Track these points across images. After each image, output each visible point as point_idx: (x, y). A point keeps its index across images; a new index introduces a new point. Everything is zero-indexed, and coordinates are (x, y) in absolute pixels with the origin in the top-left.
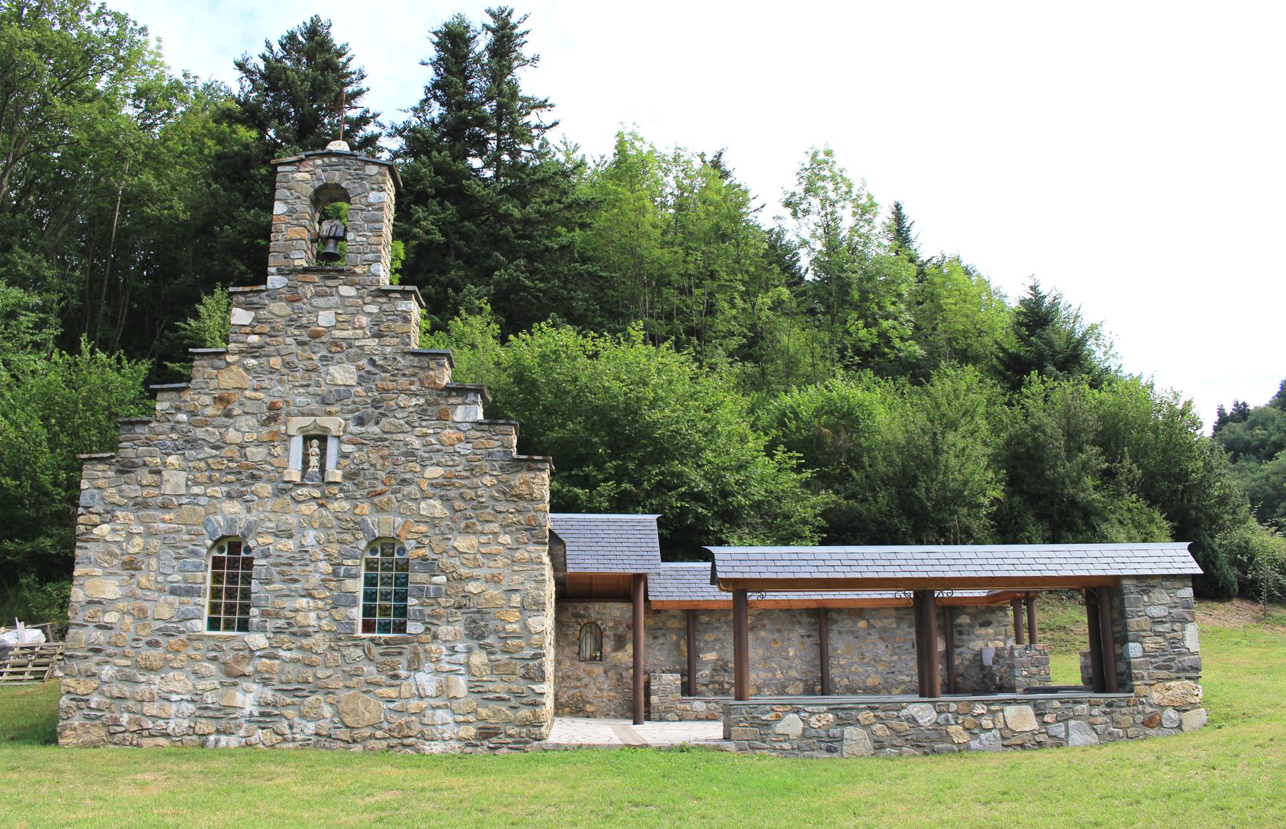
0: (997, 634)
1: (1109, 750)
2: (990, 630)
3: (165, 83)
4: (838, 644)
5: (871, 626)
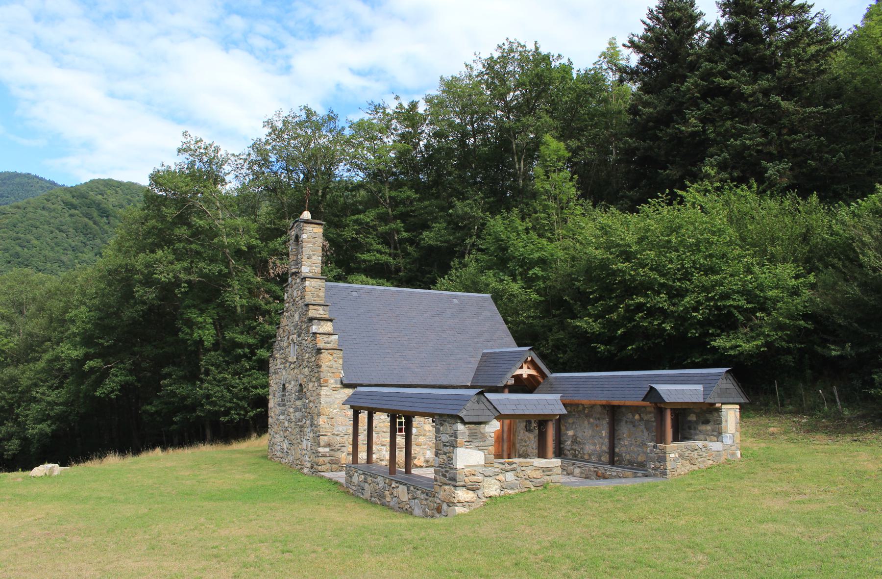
0: (713, 431)
1: (425, 520)
2: (709, 428)
3: (634, 59)
4: (624, 430)
5: (641, 419)
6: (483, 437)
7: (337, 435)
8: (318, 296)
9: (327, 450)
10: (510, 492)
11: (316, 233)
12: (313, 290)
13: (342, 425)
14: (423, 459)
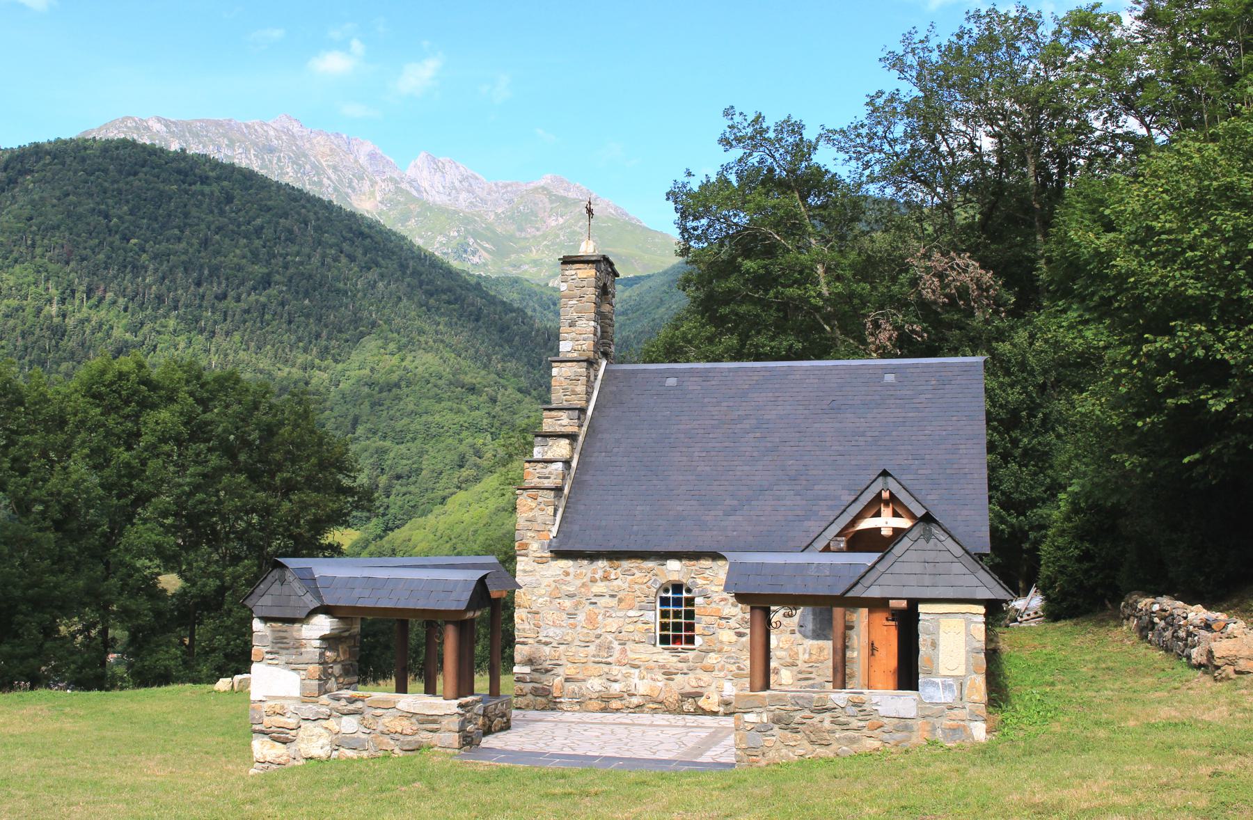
6: (298, 646)
7: (546, 644)
8: (574, 393)
9: (527, 669)
10: (350, 753)
11: (583, 280)
12: (565, 383)
13: (554, 625)
14: (715, 698)
